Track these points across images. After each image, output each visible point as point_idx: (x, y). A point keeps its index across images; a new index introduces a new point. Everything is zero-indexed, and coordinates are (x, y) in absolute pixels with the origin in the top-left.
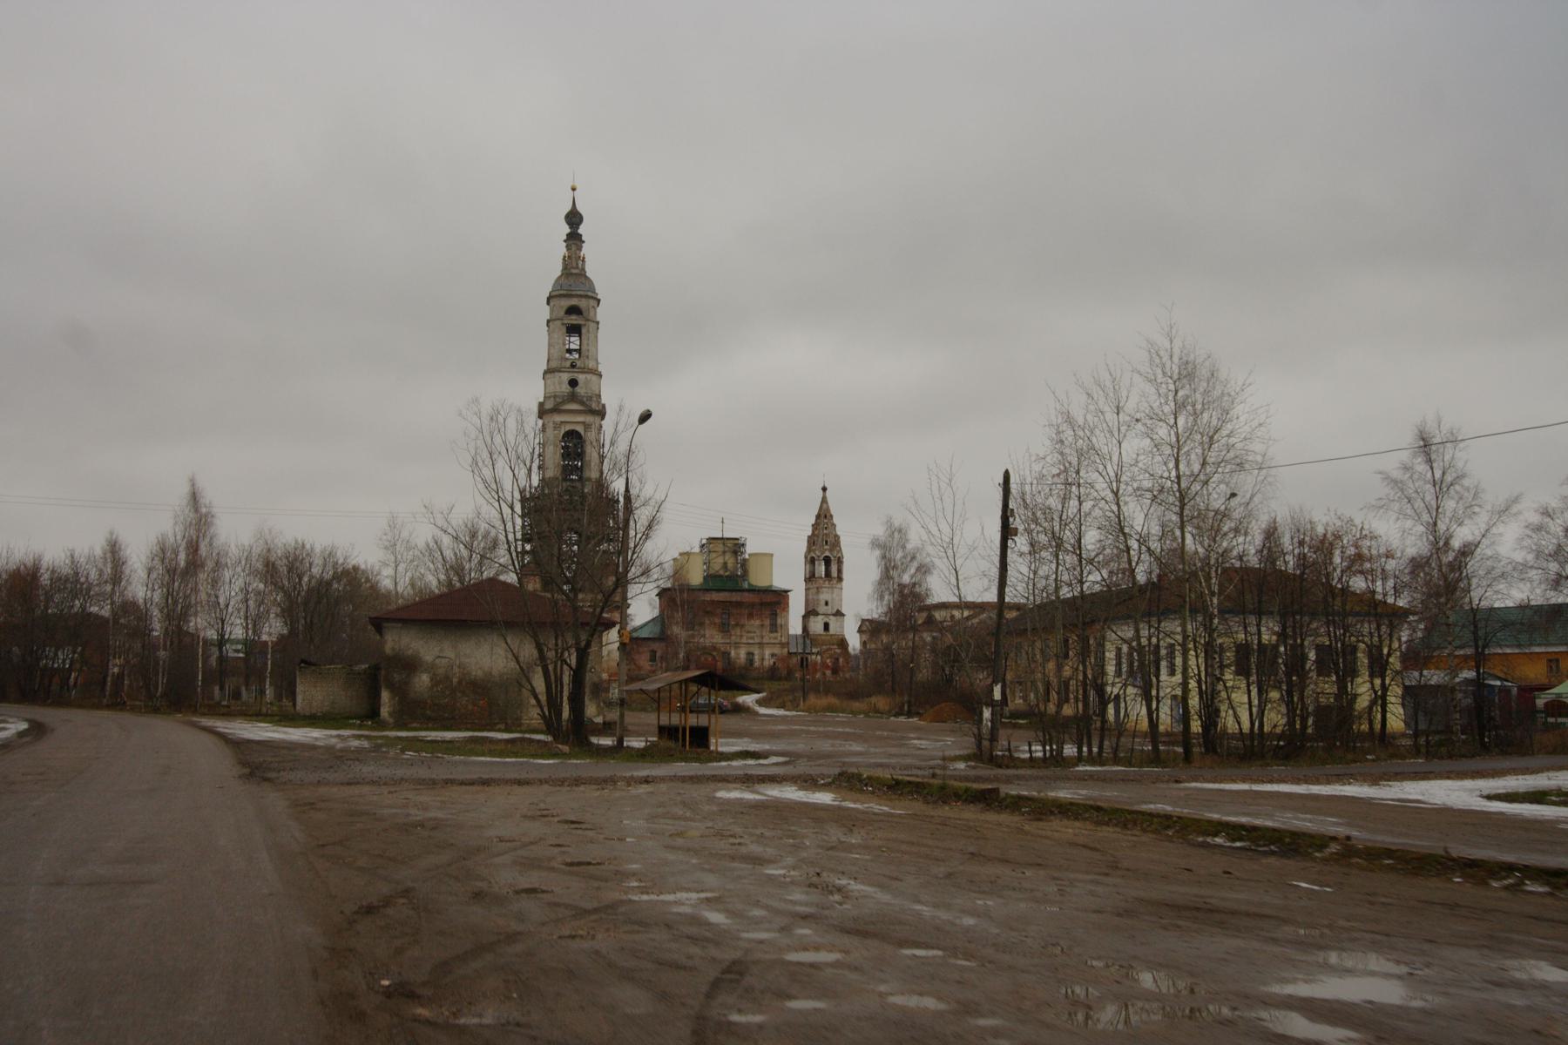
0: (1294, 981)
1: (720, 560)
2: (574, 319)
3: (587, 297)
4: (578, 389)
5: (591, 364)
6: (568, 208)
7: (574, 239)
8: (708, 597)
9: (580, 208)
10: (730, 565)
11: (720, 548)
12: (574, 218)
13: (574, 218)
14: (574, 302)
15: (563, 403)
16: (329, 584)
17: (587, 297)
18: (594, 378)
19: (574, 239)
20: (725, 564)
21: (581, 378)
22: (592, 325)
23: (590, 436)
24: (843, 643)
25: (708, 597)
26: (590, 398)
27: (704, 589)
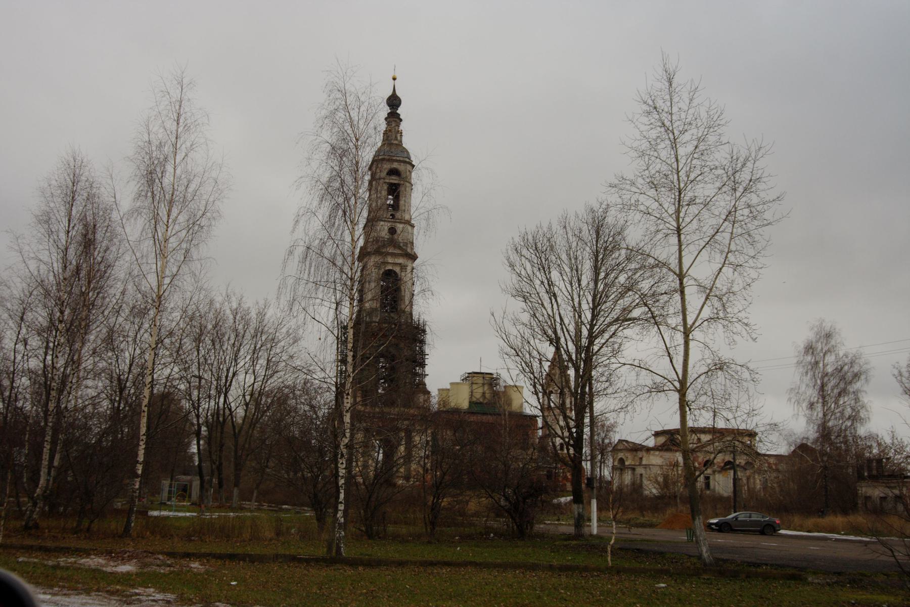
0: (87, 553)
1: (480, 390)
2: (394, 180)
3: (405, 162)
4: (396, 237)
5: (407, 217)
6: (390, 93)
7: (394, 117)
8: (473, 418)
9: (398, 93)
10: (487, 395)
11: (480, 381)
12: (394, 102)
13: (394, 102)
14: (395, 165)
15: (384, 246)
16: (583, 488)
17: (405, 162)
18: (410, 228)
19: (394, 117)
20: (484, 393)
21: (400, 227)
22: (408, 184)
23: (406, 276)
24: (700, 557)
25: (473, 418)
26: (406, 244)
27: (470, 412)
